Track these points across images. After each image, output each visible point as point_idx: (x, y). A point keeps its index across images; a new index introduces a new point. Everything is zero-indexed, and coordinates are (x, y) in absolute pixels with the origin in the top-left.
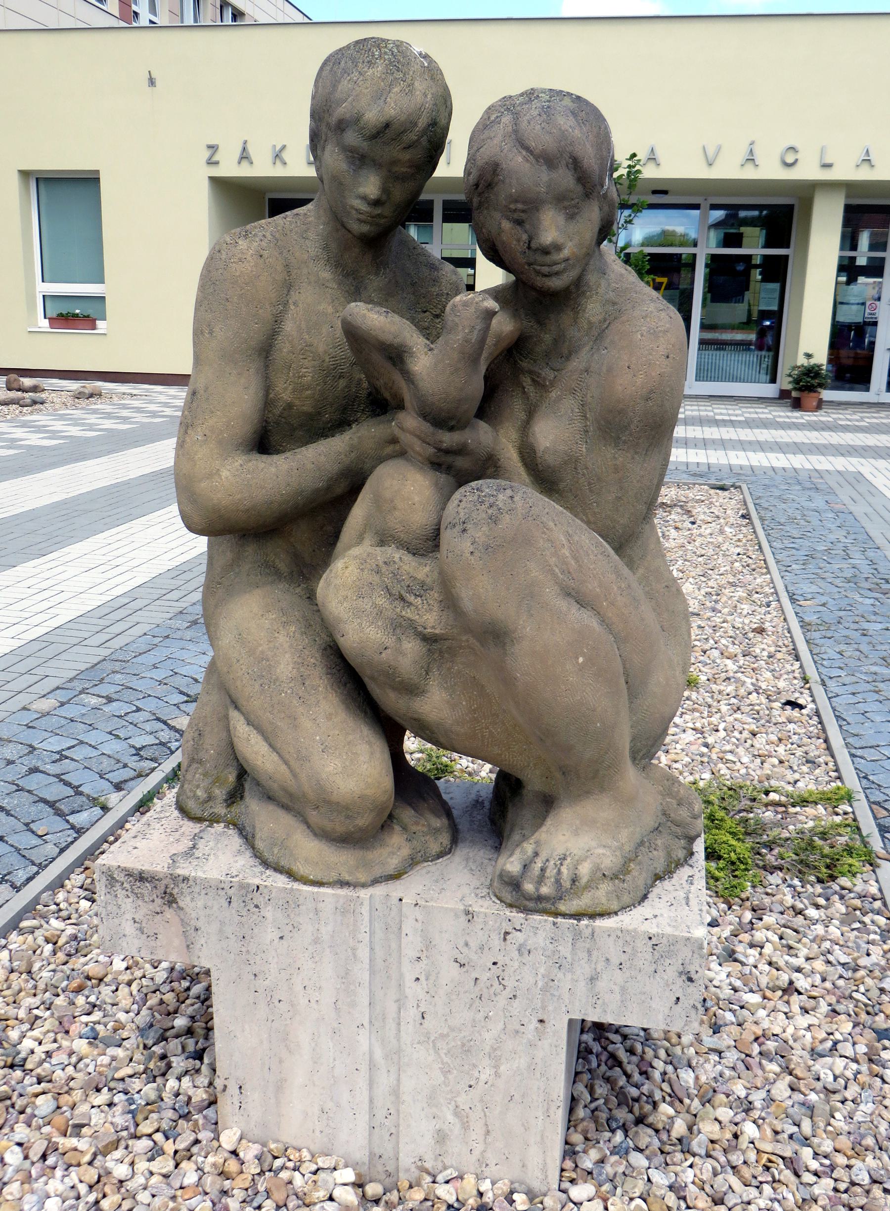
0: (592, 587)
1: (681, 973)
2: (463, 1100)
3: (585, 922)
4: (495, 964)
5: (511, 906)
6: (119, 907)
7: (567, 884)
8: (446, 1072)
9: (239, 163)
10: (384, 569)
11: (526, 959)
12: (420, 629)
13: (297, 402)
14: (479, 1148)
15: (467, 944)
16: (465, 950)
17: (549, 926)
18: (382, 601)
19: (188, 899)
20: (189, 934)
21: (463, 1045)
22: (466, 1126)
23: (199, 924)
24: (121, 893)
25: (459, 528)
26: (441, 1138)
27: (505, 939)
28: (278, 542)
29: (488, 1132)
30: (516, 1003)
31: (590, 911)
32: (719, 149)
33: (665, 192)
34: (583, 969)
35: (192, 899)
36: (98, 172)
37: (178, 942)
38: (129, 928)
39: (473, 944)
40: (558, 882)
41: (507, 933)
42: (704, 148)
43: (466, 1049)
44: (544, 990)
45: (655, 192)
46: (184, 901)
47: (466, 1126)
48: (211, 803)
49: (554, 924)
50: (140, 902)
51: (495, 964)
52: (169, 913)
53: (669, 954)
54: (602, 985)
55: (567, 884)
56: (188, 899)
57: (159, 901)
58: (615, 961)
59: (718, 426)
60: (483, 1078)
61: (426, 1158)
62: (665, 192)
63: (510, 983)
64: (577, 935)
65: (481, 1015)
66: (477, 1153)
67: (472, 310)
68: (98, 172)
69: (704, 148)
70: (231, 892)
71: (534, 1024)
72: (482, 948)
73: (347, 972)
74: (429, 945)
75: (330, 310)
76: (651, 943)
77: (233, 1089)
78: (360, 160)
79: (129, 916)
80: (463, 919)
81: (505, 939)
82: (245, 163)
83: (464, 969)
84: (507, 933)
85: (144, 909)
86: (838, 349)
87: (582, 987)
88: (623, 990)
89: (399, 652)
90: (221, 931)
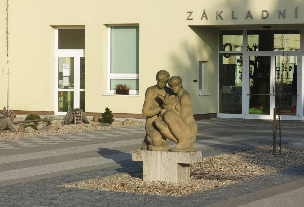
2: (167, 174)
8: (166, 171)
9: (246, 18)
11: (173, 157)
14: (169, 179)
22: (168, 177)
26: (165, 179)
28: (25, 120)
32: (285, 11)
34: (178, 158)
36: (139, 24)
42: (296, 10)
43: (168, 168)
44: (175, 160)
47: (168, 177)
54: (180, 159)
64: (177, 154)
68: (139, 24)
69: (296, 10)
73: (156, 160)
74: (164, 156)
77: (145, 176)
79: (135, 156)
82: (249, 18)
87: (178, 160)
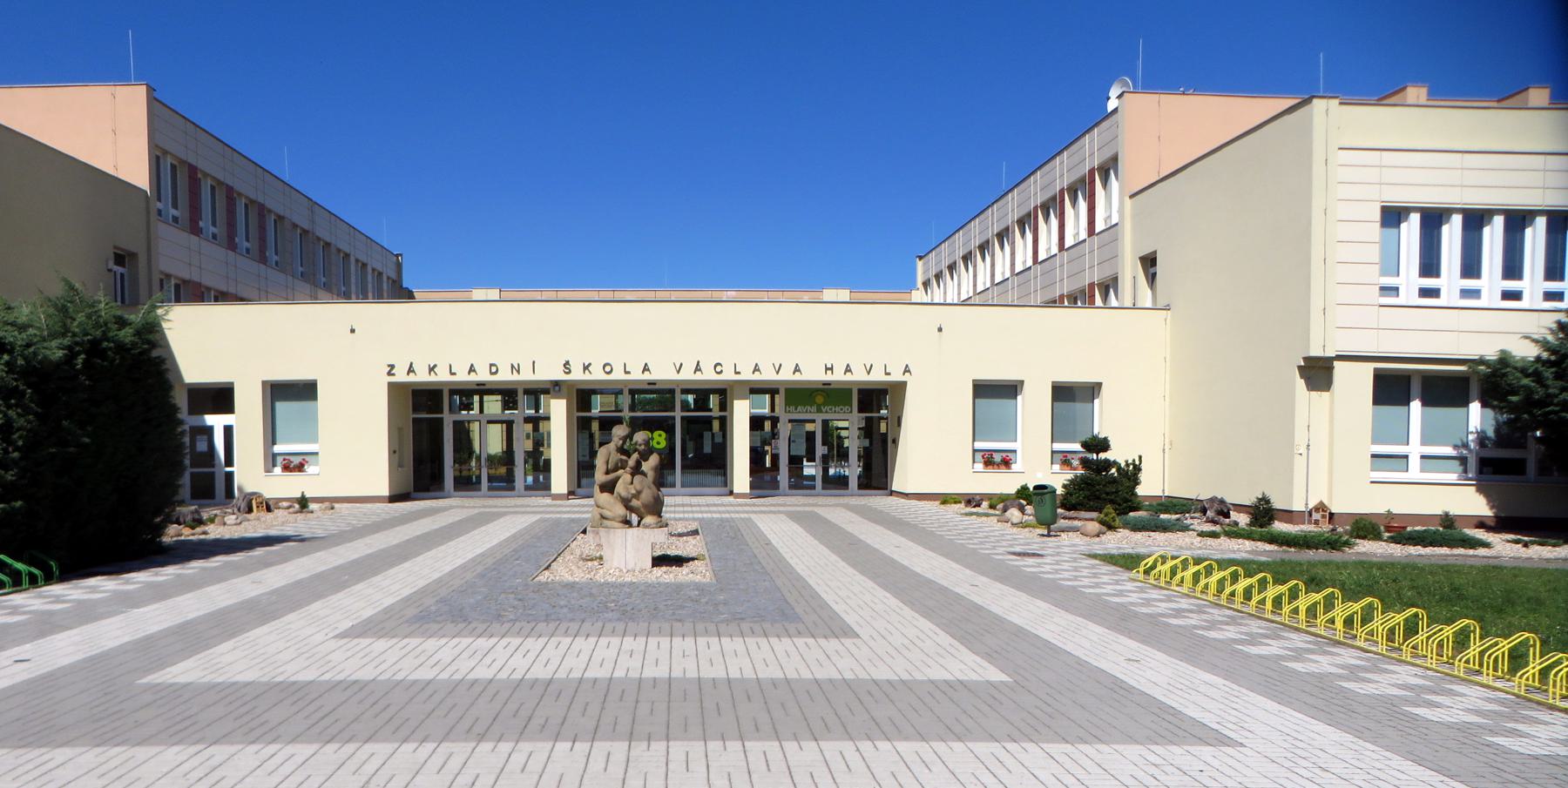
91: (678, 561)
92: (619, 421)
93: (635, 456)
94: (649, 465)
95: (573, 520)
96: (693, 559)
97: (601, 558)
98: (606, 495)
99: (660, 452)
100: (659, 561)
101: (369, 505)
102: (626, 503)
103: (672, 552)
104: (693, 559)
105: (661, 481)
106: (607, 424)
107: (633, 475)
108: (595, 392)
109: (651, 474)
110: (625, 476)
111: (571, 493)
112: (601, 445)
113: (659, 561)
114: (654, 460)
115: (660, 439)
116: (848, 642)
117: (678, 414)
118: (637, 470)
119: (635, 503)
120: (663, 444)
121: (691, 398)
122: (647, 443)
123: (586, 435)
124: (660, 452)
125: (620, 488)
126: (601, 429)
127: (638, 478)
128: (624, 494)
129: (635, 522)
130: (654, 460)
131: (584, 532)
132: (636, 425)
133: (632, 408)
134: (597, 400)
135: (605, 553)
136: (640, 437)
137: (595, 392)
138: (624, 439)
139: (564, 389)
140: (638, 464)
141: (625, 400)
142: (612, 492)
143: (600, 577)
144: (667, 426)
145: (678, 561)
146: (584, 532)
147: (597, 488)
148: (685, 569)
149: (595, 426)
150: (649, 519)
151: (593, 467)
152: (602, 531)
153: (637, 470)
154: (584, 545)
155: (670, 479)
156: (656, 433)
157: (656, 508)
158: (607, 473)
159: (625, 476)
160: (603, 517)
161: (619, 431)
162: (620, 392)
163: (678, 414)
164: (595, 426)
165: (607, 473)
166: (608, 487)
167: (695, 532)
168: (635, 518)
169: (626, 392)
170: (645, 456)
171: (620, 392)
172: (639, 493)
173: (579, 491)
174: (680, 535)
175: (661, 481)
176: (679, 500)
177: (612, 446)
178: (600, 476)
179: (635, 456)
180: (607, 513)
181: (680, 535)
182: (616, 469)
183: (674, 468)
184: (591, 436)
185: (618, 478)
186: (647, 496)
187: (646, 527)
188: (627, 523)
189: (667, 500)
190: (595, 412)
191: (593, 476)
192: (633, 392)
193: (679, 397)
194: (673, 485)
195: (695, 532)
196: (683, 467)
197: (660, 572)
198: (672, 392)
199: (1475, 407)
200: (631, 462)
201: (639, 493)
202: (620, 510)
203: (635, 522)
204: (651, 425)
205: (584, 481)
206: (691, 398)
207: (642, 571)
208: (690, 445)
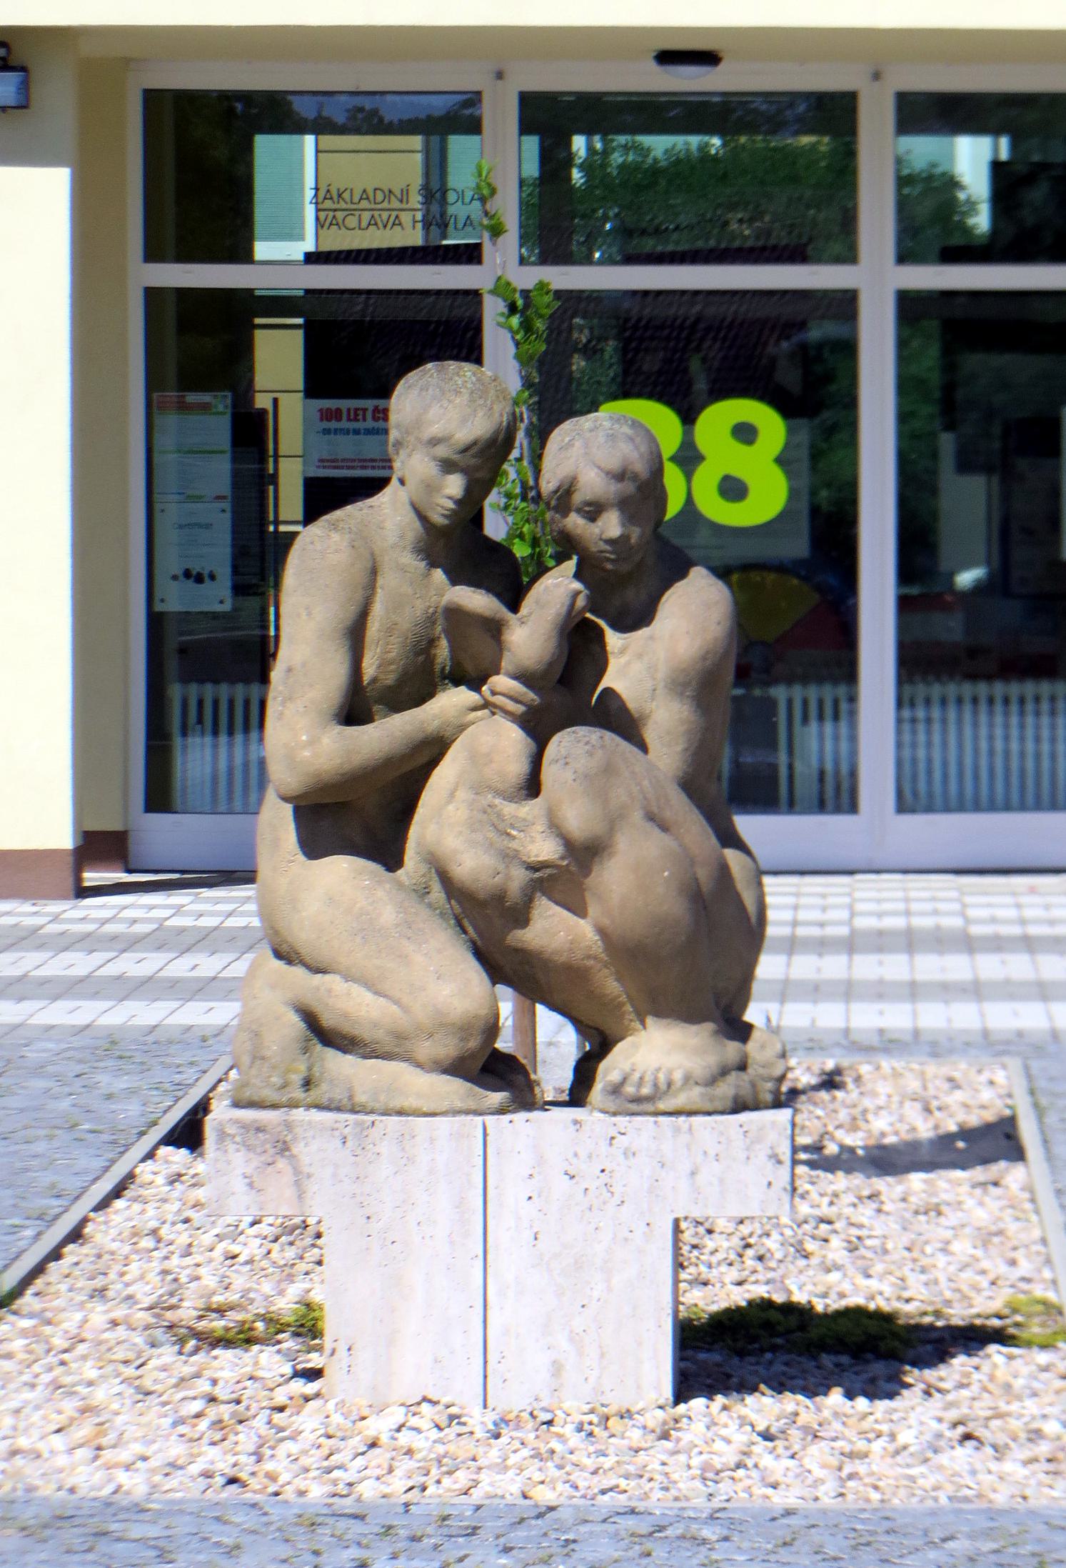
0: (667, 814)
1: (770, 1157)
3: (682, 1119)
4: (603, 1171)
5: (615, 1114)
6: (229, 1163)
7: (663, 1087)
10: (489, 810)
11: (632, 1161)
12: (525, 858)
13: (382, 676)
15: (576, 1155)
16: (574, 1161)
17: (651, 1125)
18: (492, 834)
19: (302, 1144)
20: (300, 1181)
21: (576, 1262)
23: (312, 1170)
24: (231, 1147)
25: (562, 762)
26: (557, 1369)
27: (611, 1144)
29: (602, 1355)
30: (624, 1208)
31: (688, 1108)
33: (708, 58)
35: (306, 1145)
37: (290, 1192)
38: (239, 1185)
39: (583, 1154)
40: (656, 1085)
41: (612, 1138)
45: (667, 57)
46: (298, 1149)
48: (287, 1089)
49: (656, 1122)
50: (252, 1155)
51: (603, 1171)
52: (282, 1164)
53: (758, 1140)
54: (700, 1178)
55: (663, 1087)
56: (302, 1144)
57: (272, 1151)
58: (712, 1153)
59: (986, 1033)
60: (596, 1294)
61: (542, 1396)
62: (708, 58)
63: (617, 1189)
64: (677, 1130)
65: (593, 1226)
66: (592, 1380)
67: (562, 590)
70: (347, 1131)
71: (643, 1227)
72: (590, 1157)
75: (410, 591)
76: (742, 1130)
78: (448, 466)
80: (573, 1128)
81: (611, 1144)
83: (574, 1181)
84: (612, 1138)
85: (256, 1161)
86: (532, 556)
88: (721, 1181)
89: (508, 877)
90: (334, 1175)
91: (869, 1350)
92: (447, 332)
93: (557, 589)
94: (655, 659)
95: (112, 1048)
96: (973, 1338)
97: (308, 1327)
98: (342, 871)
99: (742, 567)
100: (734, 1349)
101: (346, 246)
102: (489, 927)
103: (824, 1286)
104: (973, 1338)
105: (745, 769)
106: (364, 348)
107: (539, 727)
108: (276, 112)
109: (668, 722)
110: (481, 737)
111: (100, 846)
112: (325, 496)
113: (734, 1349)
114: (693, 614)
115: (741, 462)
116: (655, 810)
117: (877, 277)
118: (569, 692)
119: (553, 929)
120: (769, 495)
121: (971, 159)
122: (643, 493)
123: (217, 427)
124: (742, 567)
125: (446, 820)
126: (315, 385)
127: (573, 748)
128: (473, 863)
129: (555, 1072)
130: (693, 614)
131: (188, 1134)
132: (592, 355)
133: (555, 224)
134: (293, 174)
135: (342, 1293)
136: (594, 448)
137: (276, 112)
138: (483, 462)
139: (58, 94)
140: (580, 647)
141: (498, 162)
142: (386, 851)
143: (297, 1471)
144: (797, 367)
145: (869, 1350)
146: (188, 1134)
147: (277, 825)
148: (915, 1413)
149: (278, 358)
150: (657, 1050)
151: (251, 656)
152: (315, 1131)
153: (569, 692)
154: (199, 1224)
155: (813, 745)
156: (719, 418)
157: (704, 963)
158: (355, 709)
159: (481, 737)
160: (321, 1033)
161: (438, 410)
162: (462, 117)
163: (877, 277)
164: (278, 358)
165: (355, 709)
166: (364, 817)
167: (995, 1142)
168: (556, 1042)
169: (501, 114)
170: (623, 589)
171: (462, 117)
172: (584, 854)
173: (162, 834)
174: (886, 1160)
175: (745, 769)
176: (878, 901)
177: (388, 517)
178: (301, 733)
179: (557, 589)
180: (349, 1003)
181: (886, 1160)
182: (415, 685)
183: (845, 668)
184: (251, 432)
185: (432, 750)
186: (640, 877)
187: (639, 1102)
188: (498, 1073)
189: (786, 903)
190: (282, 252)
191: (252, 719)
192: (548, 117)
193: (882, 153)
194: (838, 795)
195: (995, 1142)
196: (916, 662)
197: (728, 1425)
198: (834, 112)
199: (611, 343)
200: (530, 634)
201: (584, 854)
202: (446, 983)
203: (555, 1072)
204: (673, 357)
205: (196, 759)
206: (971, 159)
207: (600, 1421)
208: (966, 501)
